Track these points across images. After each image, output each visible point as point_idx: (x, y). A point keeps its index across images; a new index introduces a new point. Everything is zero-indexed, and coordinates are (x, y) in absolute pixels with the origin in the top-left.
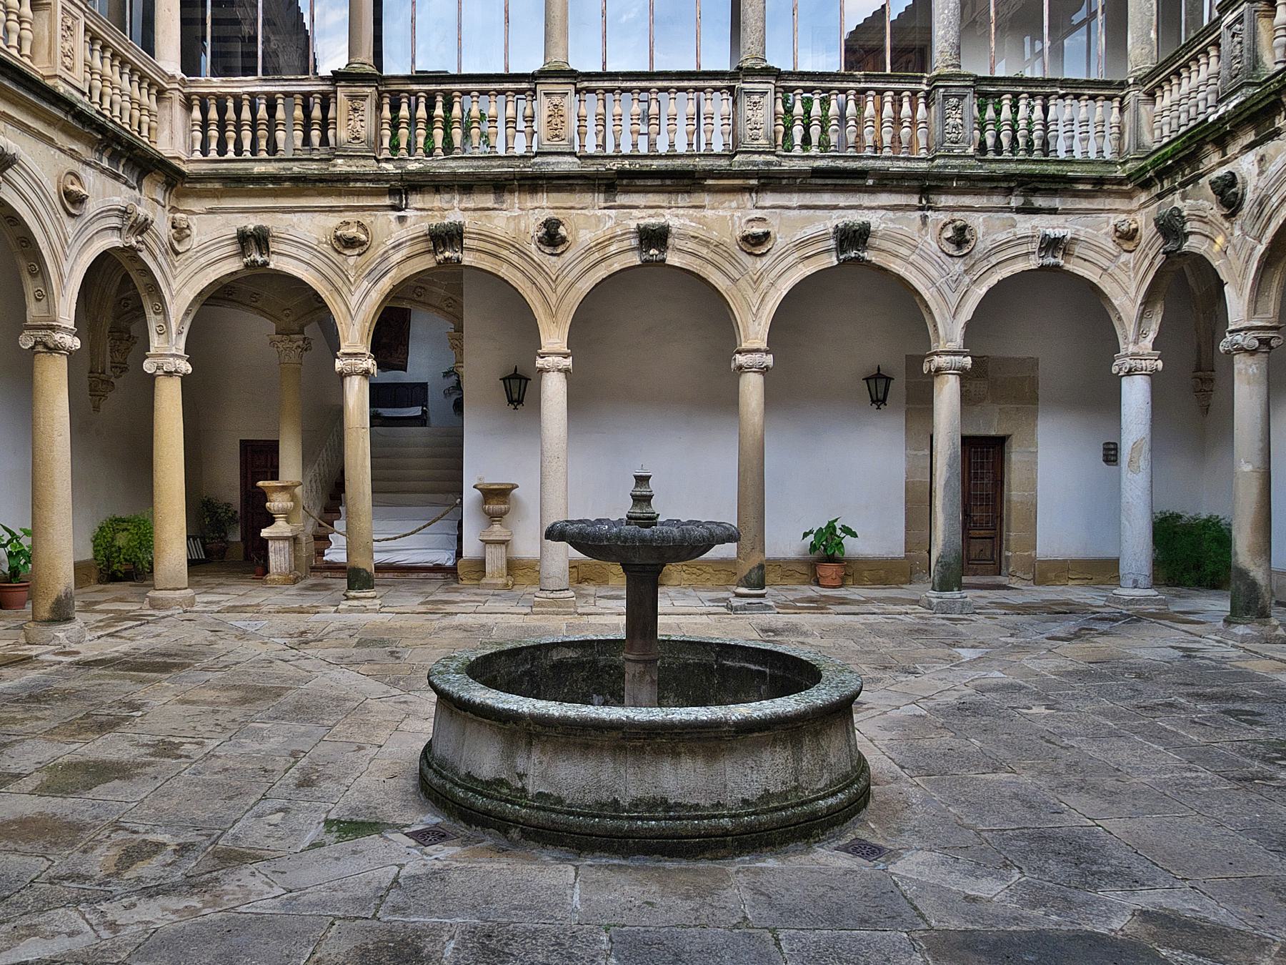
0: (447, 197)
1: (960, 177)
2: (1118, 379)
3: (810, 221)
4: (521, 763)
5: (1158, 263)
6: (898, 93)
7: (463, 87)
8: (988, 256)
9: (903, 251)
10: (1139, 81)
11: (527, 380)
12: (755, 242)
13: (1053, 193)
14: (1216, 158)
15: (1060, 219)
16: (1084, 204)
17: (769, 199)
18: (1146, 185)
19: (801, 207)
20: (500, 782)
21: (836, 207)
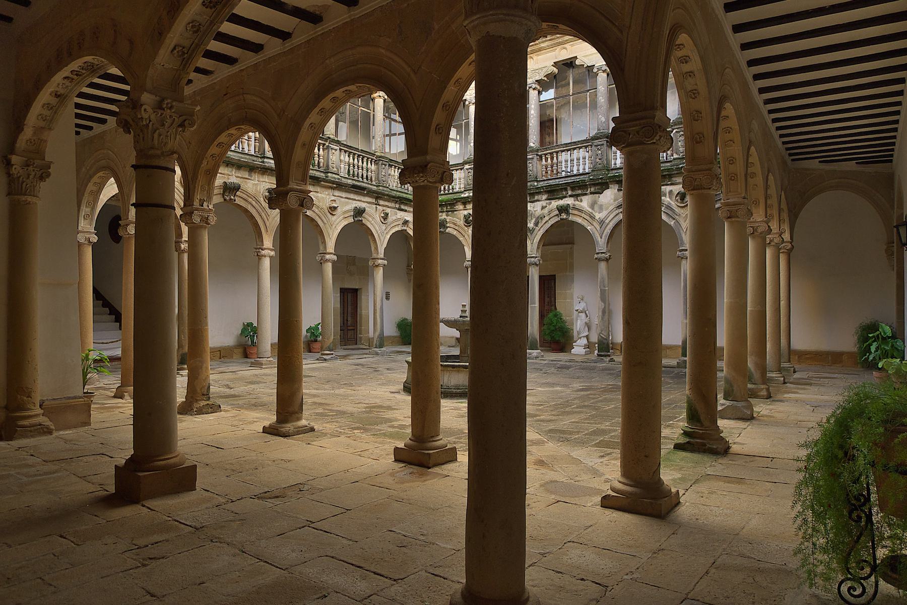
1: (387, 195)
3: (347, 203)
8: (392, 222)
13: (406, 204)
14: (461, 207)
17: (337, 193)
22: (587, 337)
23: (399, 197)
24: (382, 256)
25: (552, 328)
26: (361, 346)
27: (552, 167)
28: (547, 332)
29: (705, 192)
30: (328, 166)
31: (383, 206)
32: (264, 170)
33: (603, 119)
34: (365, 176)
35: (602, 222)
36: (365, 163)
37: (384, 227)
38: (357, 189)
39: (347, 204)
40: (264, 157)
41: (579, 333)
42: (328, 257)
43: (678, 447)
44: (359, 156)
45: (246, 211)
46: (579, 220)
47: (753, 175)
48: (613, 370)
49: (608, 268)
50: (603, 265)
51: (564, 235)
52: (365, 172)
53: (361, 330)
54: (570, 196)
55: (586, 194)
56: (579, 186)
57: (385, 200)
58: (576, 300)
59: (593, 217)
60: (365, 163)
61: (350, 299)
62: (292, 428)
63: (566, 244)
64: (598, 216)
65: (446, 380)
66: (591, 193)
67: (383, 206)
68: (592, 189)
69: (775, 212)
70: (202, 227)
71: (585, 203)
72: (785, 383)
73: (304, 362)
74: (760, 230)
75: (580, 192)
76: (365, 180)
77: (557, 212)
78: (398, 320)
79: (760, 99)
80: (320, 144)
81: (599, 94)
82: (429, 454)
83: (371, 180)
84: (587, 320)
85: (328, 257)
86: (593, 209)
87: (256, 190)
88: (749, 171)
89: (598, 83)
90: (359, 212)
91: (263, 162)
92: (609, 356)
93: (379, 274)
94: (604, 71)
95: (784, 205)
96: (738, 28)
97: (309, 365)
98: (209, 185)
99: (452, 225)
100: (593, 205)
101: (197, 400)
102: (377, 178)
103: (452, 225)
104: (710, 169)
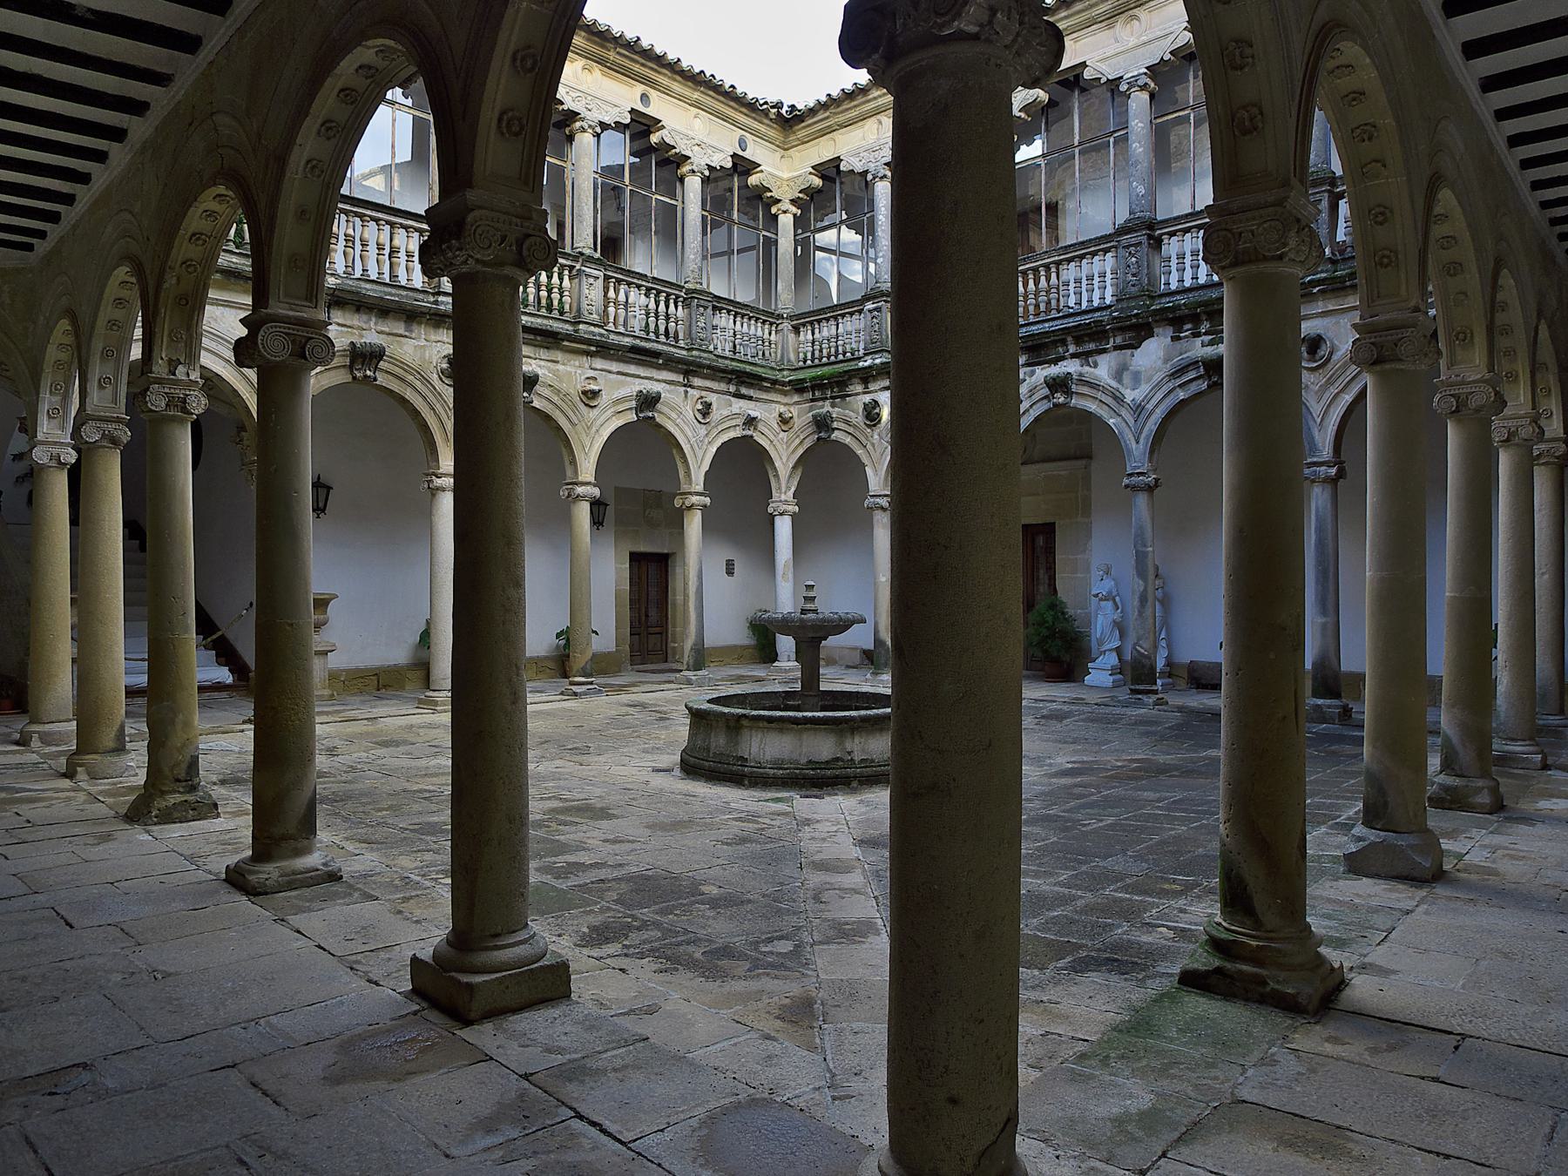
0: (365, 317)
1: (709, 367)
2: (772, 517)
3: (623, 384)
4: (848, 746)
5: (808, 444)
6: (668, 295)
7: (374, 214)
9: (674, 415)
10: (790, 318)
11: (329, 488)
12: (591, 396)
13: (750, 386)
15: (751, 404)
16: (764, 396)
17: (599, 363)
18: (800, 391)
19: (619, 373)
20: (837, 759)
21: (638, 377)
22: (1118, 650)
23: (733, 372)
24: (700, 488)
25: (1045, 632)
26: (675, 666)
27: (1036, 295)
28: (1036, 639)
29: (1270, 267)
30: (579, 310)
31: (700, 388)
32: (436, 319)
33: (1141, 190)
34: (662, 329)
35: (1138, 409)
36: (662, 305)
37: (703, 430)
38: (641, 355)
39: (621, 386)
40: (439, 293)
41: (1100, 642)
42: (580, 490)
43: (1190, 980)
44: (619, 281)
45: (403, 401)
46: (1092, 407)
47: (1507, 331)
48: (1156, 723)
49: (1152, 505)
50: (1142, 500)
51: (1074, 437)
52: (662, 323)
53: (674, 634)
54: (1074, 356)
55: (1104, 351)
56: (1090, 334)
57: (705, 377)
58: (1096, 574)
59: (1119, 399)
60: (662, 305)
61: (652, 575)
62: (275, 875)
63: (1076, 458)
64: (1130, 395)
65: (754, 749)
66: (1116, 348)
67: (700, 388)
68: (1119, 340)
69: (1522, 367)
70: (173, 419)
71: (1103, 369)
72: (1545, 767)
73: (530, 698)
74: (1473, 404)
75: (1092, 346)
76: (662, 339)
77: (1046, 391)
78: (750, 615)
79: (1532, 200)
80: (563, 266)
81: (1132, 137)
82: (469, 986)
83: (676, 338)
84: (1117, 616)
85: (580, 490)
86: (1120, 381)
87: (422, 358)
88: (1498, 322)
89: (1131, 113)
90: (648, 402)
91: (436, 302)
92: (1155, 692)
93: (694, 525)
94: (1144, 87)
95: (1546, 353)
96: (1473, 49)
97: (544, 708)
98: (189, 328)
99: (842, 426)
100: (1118, 375)
101: (163, 793)
102: (689, 334)
103: (842, 426)
104: (1280, 203)
